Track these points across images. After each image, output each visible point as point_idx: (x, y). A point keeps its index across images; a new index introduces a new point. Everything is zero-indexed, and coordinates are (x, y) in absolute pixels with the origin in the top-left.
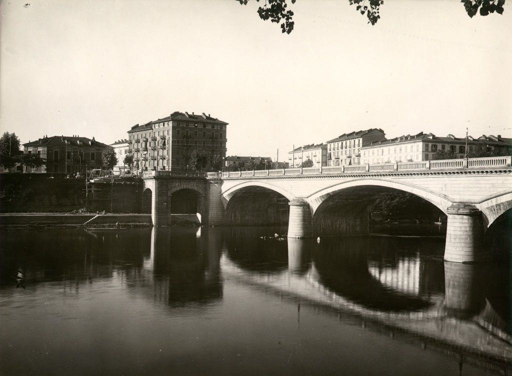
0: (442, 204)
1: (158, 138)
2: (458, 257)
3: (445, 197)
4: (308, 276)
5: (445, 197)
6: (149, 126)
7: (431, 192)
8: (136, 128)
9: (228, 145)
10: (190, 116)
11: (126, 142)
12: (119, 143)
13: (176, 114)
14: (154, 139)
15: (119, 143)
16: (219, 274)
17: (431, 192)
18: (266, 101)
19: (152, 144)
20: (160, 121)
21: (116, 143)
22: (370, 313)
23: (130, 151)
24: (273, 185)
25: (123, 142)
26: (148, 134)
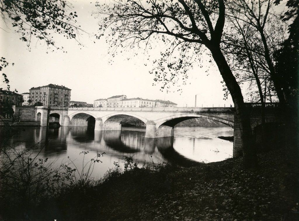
0: (145, 121)
1: (43, 93)
2: (176, 129)
3: (146, 119)
4: (93, 143)
5: (146, 119)
6: (39, 88)
7: (142, 117)
8: (33, 89)
9: (71, 97)
10: (57, 86)
11: (28, 93)
12: (25, 94)
13: (51, 85)
14: (41, 93)
15: (25, 94)
16: (65, 144)
17: (142, 117)
18: (64, 52)
19: (44, 98)
20: (43, 87)
21: (23, 94)
22: (122, 154)
23: (30, 97)
24: (89, 113)
25: (26, 93)
26: (38, 91)
